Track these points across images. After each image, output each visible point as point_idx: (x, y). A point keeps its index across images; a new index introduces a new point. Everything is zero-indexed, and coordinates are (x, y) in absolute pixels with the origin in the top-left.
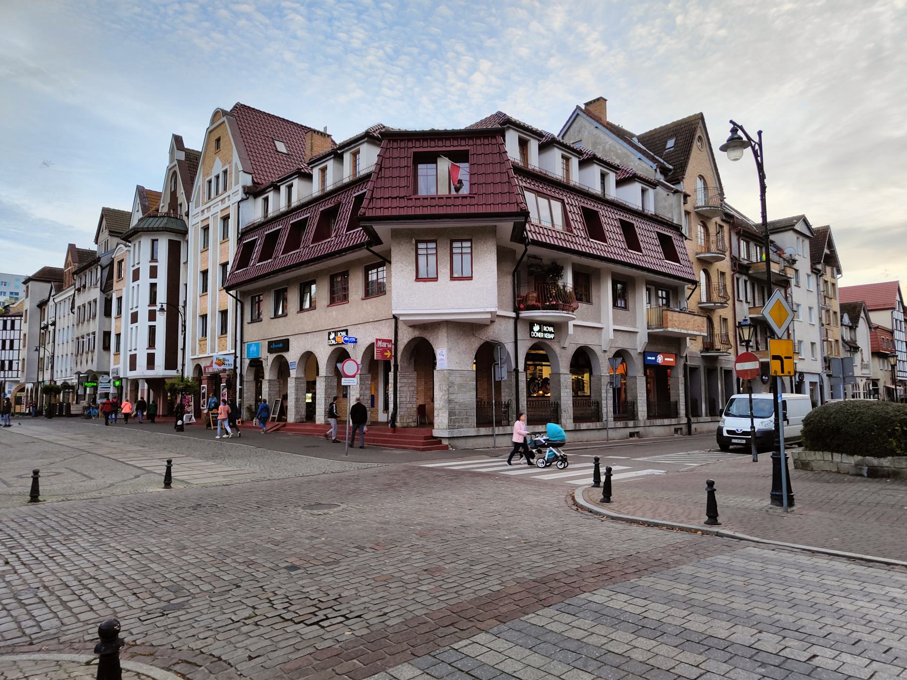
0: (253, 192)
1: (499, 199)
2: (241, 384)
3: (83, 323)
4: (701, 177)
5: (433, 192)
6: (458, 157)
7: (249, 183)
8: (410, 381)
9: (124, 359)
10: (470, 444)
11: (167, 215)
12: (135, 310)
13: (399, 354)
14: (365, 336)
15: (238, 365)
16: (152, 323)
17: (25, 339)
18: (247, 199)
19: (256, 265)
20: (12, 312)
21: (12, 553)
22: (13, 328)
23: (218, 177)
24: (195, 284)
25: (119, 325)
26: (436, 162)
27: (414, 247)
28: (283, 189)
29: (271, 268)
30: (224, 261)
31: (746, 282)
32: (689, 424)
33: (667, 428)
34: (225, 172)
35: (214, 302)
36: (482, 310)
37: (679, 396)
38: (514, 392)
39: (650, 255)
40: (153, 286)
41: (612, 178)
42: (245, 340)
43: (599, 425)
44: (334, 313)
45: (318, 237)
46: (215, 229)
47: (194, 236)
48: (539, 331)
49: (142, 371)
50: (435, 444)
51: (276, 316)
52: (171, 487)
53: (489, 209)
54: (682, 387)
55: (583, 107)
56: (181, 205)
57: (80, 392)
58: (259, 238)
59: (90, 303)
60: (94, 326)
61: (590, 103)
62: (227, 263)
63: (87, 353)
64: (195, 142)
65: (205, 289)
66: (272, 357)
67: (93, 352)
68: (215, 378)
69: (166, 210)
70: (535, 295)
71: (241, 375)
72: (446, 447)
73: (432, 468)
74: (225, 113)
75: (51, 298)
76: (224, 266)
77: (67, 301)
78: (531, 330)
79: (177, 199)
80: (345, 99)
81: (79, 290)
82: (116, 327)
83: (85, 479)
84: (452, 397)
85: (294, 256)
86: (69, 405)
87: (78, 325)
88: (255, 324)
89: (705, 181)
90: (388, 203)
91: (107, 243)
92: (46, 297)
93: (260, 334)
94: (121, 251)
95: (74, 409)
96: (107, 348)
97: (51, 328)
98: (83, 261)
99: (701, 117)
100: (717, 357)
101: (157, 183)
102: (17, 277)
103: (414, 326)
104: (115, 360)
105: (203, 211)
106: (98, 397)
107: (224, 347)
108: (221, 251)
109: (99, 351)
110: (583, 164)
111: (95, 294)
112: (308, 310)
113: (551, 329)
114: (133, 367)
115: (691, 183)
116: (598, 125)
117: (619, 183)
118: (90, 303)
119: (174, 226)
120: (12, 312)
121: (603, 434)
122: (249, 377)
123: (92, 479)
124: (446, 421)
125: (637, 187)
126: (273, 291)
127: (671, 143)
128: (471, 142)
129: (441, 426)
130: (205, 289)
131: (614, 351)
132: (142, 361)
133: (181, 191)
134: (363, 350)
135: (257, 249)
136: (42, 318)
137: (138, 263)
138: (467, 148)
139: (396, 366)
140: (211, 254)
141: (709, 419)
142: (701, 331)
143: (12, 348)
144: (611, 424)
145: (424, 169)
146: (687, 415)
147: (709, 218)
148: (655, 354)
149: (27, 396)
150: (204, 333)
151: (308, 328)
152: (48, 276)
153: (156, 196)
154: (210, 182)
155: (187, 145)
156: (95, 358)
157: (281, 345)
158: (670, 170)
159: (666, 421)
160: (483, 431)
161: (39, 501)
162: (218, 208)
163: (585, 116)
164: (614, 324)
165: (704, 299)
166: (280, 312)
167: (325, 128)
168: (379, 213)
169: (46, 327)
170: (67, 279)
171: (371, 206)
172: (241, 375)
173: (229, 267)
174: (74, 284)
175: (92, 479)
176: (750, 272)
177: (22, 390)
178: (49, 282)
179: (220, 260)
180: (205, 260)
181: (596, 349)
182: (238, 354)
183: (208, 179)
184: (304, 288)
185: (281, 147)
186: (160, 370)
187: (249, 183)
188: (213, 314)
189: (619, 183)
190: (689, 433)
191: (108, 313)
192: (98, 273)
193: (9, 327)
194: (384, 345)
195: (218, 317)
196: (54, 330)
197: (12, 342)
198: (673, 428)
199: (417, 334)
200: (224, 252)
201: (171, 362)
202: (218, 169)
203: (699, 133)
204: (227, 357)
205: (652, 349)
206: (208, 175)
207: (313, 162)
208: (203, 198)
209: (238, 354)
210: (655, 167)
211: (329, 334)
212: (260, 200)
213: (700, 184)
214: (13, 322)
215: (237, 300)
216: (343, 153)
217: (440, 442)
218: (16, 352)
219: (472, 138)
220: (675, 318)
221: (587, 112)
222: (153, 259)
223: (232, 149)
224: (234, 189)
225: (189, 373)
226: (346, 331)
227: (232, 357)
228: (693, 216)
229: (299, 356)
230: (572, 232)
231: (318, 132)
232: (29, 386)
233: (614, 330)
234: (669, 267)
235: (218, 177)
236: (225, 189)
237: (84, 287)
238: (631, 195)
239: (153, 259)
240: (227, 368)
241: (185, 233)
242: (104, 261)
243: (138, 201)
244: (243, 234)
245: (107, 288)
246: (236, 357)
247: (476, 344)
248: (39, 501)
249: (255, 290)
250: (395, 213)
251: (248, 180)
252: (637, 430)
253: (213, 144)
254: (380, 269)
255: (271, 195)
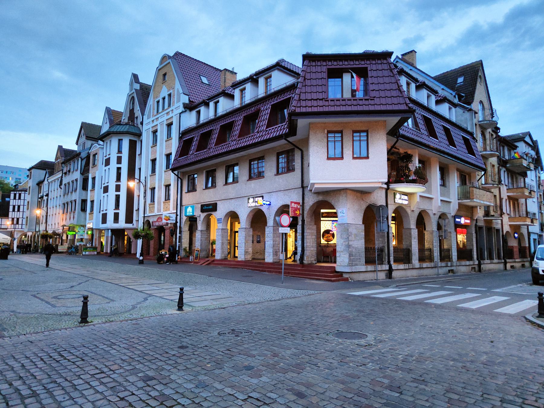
0: (190, 107)
1: (389, 101)
2: (180, 232)
3: (68, 194)
4: (481, 102)
5: (339, 96)
6: (362, 73)
7: (187, 101)
8: (312, 231)
9: (97, 216)
10: (361, 277)
11: (126, 124)
12: (106, 185)
13: (305, 213)
14: (278, 202)
15: (178, 221)
16: (118, 193)
17: (28, 205)
18: (186, 111)
19: (193, 155)
20: (20, 188)
21: (122, 399)
22: (20, 198)
23: (164, 99)
24: (147, 168)
25: (95, 195)
26: (341, 77)
27: (326, 136)
28: (212, 104)
29: (204, 153)
30: (168, 152)
31: (504, 171)
32: (479, 265)
33: (468, 267)
34: (170, 95)
35: (160, 180)
36: (376, 181)
37: (473, 246)
38: (386, 241)
39: (461, 151)
40: (119, 169)
41: (433, 98)
42: (184, 203)
43: (432, 264)
44: (253, 185)
45: (241, 135)
46: (162, 132)
47: (146, 138)
48: (400, 199)
49: (110, 224)
50: (339, 276)
51: (207, 188)
52: (182, 310)
53: (383, 108)
54: (474, 240)
55: (400, 57)
56: (137, 118)
57: (64, 237)
58: (196, 137)
59: (73, 182)
60: (76, 196)
61: (406, 54)
62: (171, 154)
63: (70, 213)
64: (147, 78)
65: (153, 170)
66: (203, 215)
67: (74, 213)
68: (161, 229)
69: (126, 121)
70: (395, 173)
71: (180, 227)
72: (347, 279)
73: (359, 296)
74: (170, 57)
75: (46, 179)
76: (168, 156)
77: (57, 181)
78: (395, 198)
79: (134, 114)
80: (247, 50)
81: (65, 173)
82: (91, 196)
83: (108, 301)
84: (351, 243)
85: (204, 154)
86: (57, 246)
87: (64, 195)
88: (191, 193)
89: (483, 105)
90: (309, 103)
91: (84, 144)
92: (42, 178)
93: (192, 204)
94: (96, 147)
95: (60, 249)
96: (84, 210)
97: (45, 198)
98: (67, 157)
99: (480, 63)
100: (492, 220)
101: (120, 105)
102: (20, 170)
103: (319, 193)
104: (89, 217)
105: (153, 121)
106: (76, 240)
107: (167, 209)
108: (166, 146)
109: (78, 213)
110: (418, 88)
111: (77, 175)
112: (231, 183)
113: (406, 197)
114: (104, 221)
115: (475, 106)
116: (411, 68)
117: (438, 102)
118: (73, 182)
119: (133, 131)
120: (20, 188)
121: (434, 271)
122: (186, 229)
123: (113, 301)
124: (347, 260)
125: (446, 106)
126: (205, 171)
127: (460, 80)
128: (368, 62)
129: (342, 263)
130: (153, 170)
131: (439, 214)
132: (110, 218)
133: (137, 108)
134: (276, 210)
135: (195, 143)
136: (39, 192)
137: (109, 155)
138: (365, 66)
139: (303, 221)
140: (160, 147)
141: (489, 261)
142: (490, 202)
143: (19, 210)
144: (440, 264)
145: (333, 83)
146: (478, 259)
147: (486, 129)
148: (460, 217)
149: (28, 240)
150: (153, 200)
151: (245, 194)
152: (43, 166)
153: (120, 114)
154: (158, 102)
155: (141, 80)
156: (76, 216)
157: (211, 207)
158: (463, 96)
159: (468, 263)
160: (370, 268)
161: (87, 322)
162: (163, 119)
163: (402, 62)
164: (441, 196)
165: (483, 183)
166: (210, 185)
167: (233, 68)
168: (304, 110)
169: (42, 197)
170: (56, 168)
171: (299, 105)
172: (180, 227)
173: (173, 157)
174: (62, 170)
175: (113, 301)
176: (508, 165)
177: (26, 236)
178: (45, 170)
179: (165, 152)
180: (155, 152)
181: (430, 212)
182: (179, 213)
183: (157, 100)
184: (229, 168)
185: (205, 80)
186: (122, 224)
187: (187, 101)
188: (160, 188)
189: (438, 102)
190: (480, 270)
191: (85, 187)
192: (79, 164)
193: (17, 198)
194: (296, 206)
195: (163, 188)
196: (47, 199)
197: (19, 207)
198: (470, 267)
199: (321, 198)
200: (169, 147)
201: (129, 219)
202: (164, 93)
203: (480, 74)
204: (171, 215)
205: (459, 214)
206: (157, 98)
207: (211, 99)
208: (153, 112)
209: (179, 213)
210: (454, 94)
211: (249, 199)
212: (194, 113)
213: (480, 107)
214: (20, 195)
215: (178, 177)
216: (258, 78)
217: (341, 276)
218: (21, 213)
219: (368, 59)
220: (477, 193)
221: (402, 59)
222: (120, 151)
223: (175, 80)
224: (176, 105)
225: (140, 226)
226: (262, 197)
227: (174, 215)
228: (478, 126)
229: (225, 214)
230: (420, 131)
231: (229, 71)
232: (30, 234)
233: (441, 200)
234: (470, 158)
235: (164, 99)
236: (169, 105)
237: (69, 171)
238: (444, 109)
239: (120, 151)
240: (169, 222)
241: (139, 135)
242: (84, 155)
243: (107, 116)
244: (183, 134)
245: (85, 171)
246: (177, 215)
247: (364, 207)
248: (87, 322)
249: (191, 171)
250: (315, 110)
251: (185, 99)
252: (452, 268)
253: (162, 77)
254: (259, 161)
255: (202, 109)
